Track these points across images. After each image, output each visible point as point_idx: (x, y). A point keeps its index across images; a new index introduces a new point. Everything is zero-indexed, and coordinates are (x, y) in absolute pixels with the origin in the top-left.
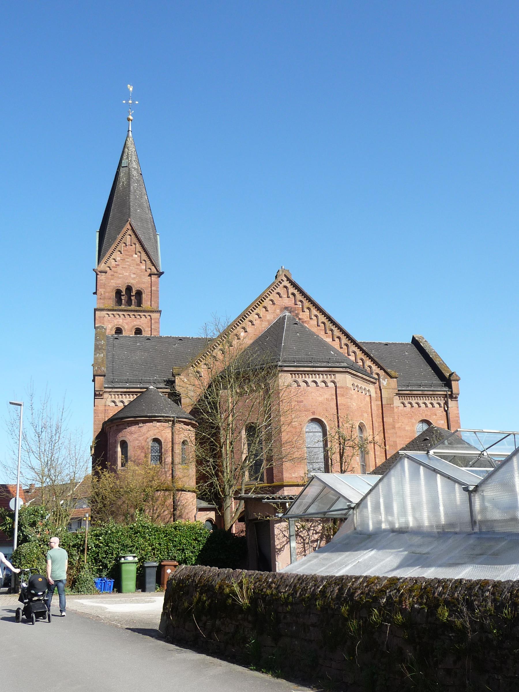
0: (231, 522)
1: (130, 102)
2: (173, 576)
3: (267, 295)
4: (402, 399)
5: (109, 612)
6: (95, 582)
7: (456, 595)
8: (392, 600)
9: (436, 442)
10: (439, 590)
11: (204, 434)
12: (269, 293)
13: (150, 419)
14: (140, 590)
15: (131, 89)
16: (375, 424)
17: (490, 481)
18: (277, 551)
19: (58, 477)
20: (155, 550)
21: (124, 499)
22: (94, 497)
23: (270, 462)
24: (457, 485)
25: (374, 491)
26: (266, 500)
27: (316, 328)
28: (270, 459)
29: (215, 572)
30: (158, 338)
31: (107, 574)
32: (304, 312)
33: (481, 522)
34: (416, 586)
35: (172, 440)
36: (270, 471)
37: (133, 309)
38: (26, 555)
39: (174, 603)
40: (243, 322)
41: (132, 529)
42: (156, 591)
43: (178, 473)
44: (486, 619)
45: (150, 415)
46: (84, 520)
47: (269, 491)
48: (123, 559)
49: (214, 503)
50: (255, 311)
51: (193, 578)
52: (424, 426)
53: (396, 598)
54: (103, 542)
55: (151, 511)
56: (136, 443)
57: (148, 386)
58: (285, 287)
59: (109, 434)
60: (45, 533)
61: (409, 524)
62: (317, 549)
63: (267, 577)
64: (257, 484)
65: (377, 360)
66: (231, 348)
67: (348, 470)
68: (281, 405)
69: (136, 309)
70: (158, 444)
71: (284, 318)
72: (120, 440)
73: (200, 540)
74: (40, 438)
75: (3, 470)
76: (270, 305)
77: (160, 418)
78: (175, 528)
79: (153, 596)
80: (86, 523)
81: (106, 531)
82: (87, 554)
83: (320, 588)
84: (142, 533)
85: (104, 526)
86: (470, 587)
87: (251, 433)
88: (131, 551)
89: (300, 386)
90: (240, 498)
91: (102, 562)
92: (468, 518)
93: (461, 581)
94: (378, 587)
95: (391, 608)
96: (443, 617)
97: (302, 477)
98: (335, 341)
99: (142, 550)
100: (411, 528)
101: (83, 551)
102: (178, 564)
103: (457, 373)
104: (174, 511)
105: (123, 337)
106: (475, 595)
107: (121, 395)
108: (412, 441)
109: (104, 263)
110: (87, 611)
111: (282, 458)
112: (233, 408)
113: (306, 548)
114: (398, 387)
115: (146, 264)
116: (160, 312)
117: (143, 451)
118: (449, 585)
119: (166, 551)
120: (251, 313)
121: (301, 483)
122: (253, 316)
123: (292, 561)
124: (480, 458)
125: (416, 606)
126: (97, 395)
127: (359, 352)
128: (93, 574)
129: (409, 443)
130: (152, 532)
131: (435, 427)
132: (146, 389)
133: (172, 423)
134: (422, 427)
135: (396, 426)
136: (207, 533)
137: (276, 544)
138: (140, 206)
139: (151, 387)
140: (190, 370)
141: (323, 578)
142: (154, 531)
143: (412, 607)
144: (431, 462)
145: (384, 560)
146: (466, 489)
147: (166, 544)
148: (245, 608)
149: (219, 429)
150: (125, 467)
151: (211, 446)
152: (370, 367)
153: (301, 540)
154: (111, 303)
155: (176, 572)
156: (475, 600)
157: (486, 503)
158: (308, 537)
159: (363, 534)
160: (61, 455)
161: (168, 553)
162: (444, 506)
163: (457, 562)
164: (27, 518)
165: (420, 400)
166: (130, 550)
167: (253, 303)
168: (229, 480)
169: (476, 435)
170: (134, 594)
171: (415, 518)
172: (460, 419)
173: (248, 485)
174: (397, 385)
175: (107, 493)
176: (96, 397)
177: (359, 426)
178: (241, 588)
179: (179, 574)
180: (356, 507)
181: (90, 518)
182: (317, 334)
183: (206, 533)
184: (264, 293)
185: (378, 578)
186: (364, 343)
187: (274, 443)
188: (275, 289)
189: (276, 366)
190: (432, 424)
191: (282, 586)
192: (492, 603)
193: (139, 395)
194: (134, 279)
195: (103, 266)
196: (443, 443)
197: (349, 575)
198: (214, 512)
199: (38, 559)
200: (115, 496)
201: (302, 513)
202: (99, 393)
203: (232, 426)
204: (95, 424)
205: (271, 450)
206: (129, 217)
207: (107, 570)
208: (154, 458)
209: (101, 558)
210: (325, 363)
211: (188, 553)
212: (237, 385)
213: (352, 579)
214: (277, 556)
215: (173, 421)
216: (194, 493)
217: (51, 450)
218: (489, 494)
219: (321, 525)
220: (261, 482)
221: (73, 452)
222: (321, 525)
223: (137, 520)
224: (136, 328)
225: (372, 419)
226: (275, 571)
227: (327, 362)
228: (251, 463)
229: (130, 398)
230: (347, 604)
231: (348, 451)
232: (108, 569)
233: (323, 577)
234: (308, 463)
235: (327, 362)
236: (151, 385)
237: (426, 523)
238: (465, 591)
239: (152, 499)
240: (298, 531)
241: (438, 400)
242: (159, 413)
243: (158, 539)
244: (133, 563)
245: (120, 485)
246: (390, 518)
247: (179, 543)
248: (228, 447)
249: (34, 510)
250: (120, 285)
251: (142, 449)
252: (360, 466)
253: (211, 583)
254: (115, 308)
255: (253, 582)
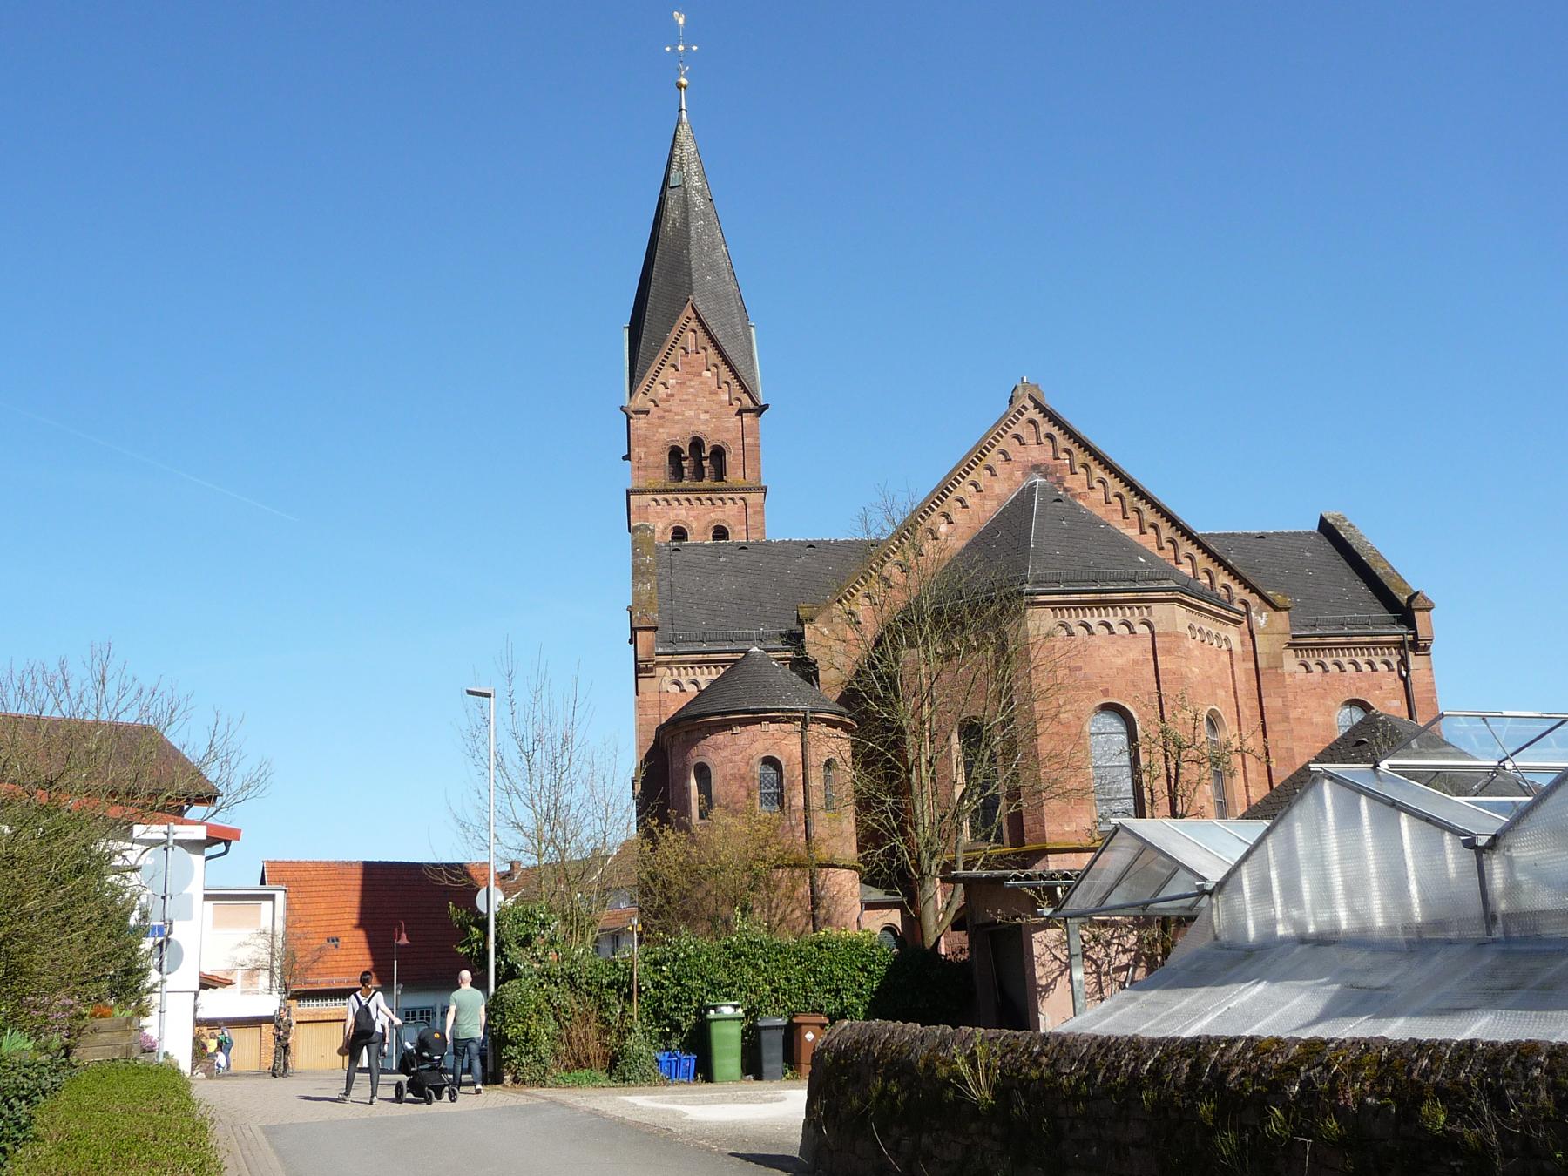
0: (936, 931)
1: (681, 48)
2: (824, 1044)
3: (992, 441)
4: (1303, 656)
5: (692, 1122)
6: (657, 1060)
7: (1462, 1076)
8: (1314, 1087)
9: (1384, 747)
10: (1422, 1065)
11: (871, 744)
12: (996, 436)
13: (755, 716)
14: (751, 1077)
15: (681, 21)
16: (1243, 712)
17: (1525, 824)
18: (1041, 992)
19: (571, 844)
20: (778, 993)
21: (707, 885)
22: (647, 883)
23: (1015, 801)
24: (1447, 837)
25: (1253, 859)
26: (1012, 882)
27: (1103, 508)
28: (1014, 795)
29: (914, 1033)
30: (762, 544)
31: (681, 1044)
32: (1076, 473)
33: (1506, 916)
34: (1366, 1058)
35: (803, 760)
36: (1016, 820)
37: (708, 486)
38: (514, 1004)
39: (829, 1101)
40: (942, 501)
41: (729, 948)
42: (784, 1078)
43: (819, 830)
44: (1537, 1129)
45: (755, 707)
46: (628, 931)
47: (1016, 863)
48: (712, 1012)
49: (898, 891)
50: (969, 478)
51: (867, 1047)
52: (1354, 714)
53: (1324, 1084)
54: (670, 976)
55: (766, 910)
56: (729, 769)
57: (747, 647)
58: (1032, 422)
59: (671, 752)
60: (550, 958)
61: (1340, 924)
62: (1127, 985)
63: (1029, 1043)
64: (990, 848)
65: (1241, 571)
66: (920, 558)
67: (1190, 814)
68: (1033, 677)
69: (713, 487)
70: (775, 769)
71: (1032, 488)
72: (694, 764)
73: (872, 969)
74: (531, 762)
75: (460, 831)
76: (1000, 462)
77: (777, 714)
78: (819, 946)
79: (779, 1089)
80: (633, 937)
81: (675, 954)
82: (638, 1001)
83: (1149, 1063)
84: (750, 957)
85: (670, 944)
86: (1494, 1058)
87: (972, 740)
88: (728, 995)
89: (1073, 634)
90: (955, 880)
91: (669, 1019)
92: (1475, 908)
93: (1471, 1044)
94: (1280, 1061)
95: (1311, 1105)
96: (1435, 1124)
97: (1089, 830)
98: (1145, 533)
99: (751, 992)
100: (1346, 933)
101: (629, 997)
102: (827, 1021)
103: (1426, 594)
104: (812, 909)
105: (689, 545)
106: (1508, 1075)
107: (692, 668)
108: (1328, 747)
109: (644, 393)
110: (645, 1119)
111: (1040, 792)
112: (931, 687)
113: (1103, 985)
114: (1292, 630)
115: (729, 389)
116: (764, 490)
117: (744, 784)
118: (1445, 1054)
119: (802, 994)
120: (959, 483)
121: (1086, 842)
122: (964, 490)
123: (1077, 1010)
124: (1497, 775)
125: (1369, 1100)
126: (642, 670)
127: (1201, 555)
128: (652, 1043)
129: (1322, 752)
130: (770, 955)
131: (1381, 715)
132: (743, 655)
133: (800, 723)
134: (1347, 719)
135: (1291, 716)
136: (887, 955)
137: (1037, 976)
138: (713, 267)
139: (755, 649)
140: (834, 610)
141: (1154, 1043)
142: (774, 953)
143: (1361, 1103)
144: (1385, 785)
145: (1287, 1003)
146: (1470, 844)
147: (800, 980)
148: (983, 1109)
149: (904, 733)
150: (709, 819)
151: (886, 769)
152: (1226, 587)
153: (1091, 966)
154: (661, 477)
155: (829, 1034)
156: (1508, 1086)
157: (1518, 875)
158: (1107, 959)
159: (1234, 949)
160: (576, 797)
161: (806, 997)
162: (1419, 883)
163: (1457, 1004)
164: (513, 928)
165: (1344, 655)
166: (727, 993)
167: (963, 460)
168: (928, 841)
169: (1488, 725)
170: (740, 1085)
171: (1353, 911)
172: (1438, 696)
173: (970, 851)
174: (1288, 625)
175: (672, 875)
176: (639, 675)
177: (1207, 717)
178: (974, 1065)
179: (837, 1039)
180: (1216, 890)
181: (640, 928)
182: (1106, 520)
183: (885, 954)
184: (986, 436)
185: (1278, 1041)
186: (1210, 535)
187: (1022, 759)
188: (1010, 428)
189: (1020, 593)
190: (1373, 709)
191: (1062, 1060)
192: (1548, 1093)
193: (728, 667)
194: (706, 422)
195: (640, 400)
196: (1407, 745)
197: (1212, 1034)
198: (899, 911)
199: (539, 1013)
200: (690, 881)
201: (1093, 906)
202: (647, 665)
203: (931, 726)
204: (639, 731)
205: (1016, 774)
206: (691, 293)
207: (681, 1036)
208: (767, 799)
209: (666, 1010)
210: (1126, 584)
211: (847, 999)
212: (936, 637)
213: (1219, 1044)
214: (1040, 1001)
215: (804, 721)
216: (855, 872)
217: (555, 786)
218: (1524, 854)
219: (1135, 932)
220: (996, 845)
221: (599, 790)
222: (1135, 932)
223: (737, 929)
224: (715, 527)
225: (1237, 703)
226: (1038, 1028)
227: (1131, 580)
228: (975, 803)
229: (710, 673)
230: (1210, 1098)
231: (1189, 772)
232: (682, 1033)
233: (1154, 1039)
234: (1098, 800)
235: (1131, 580)
236: (754, 644)
237: (1380, 922)
238: (1484, 1066)
239: (767, 886)
240: (1084, 946)
241: (1384, 654)
242: (774, 704)
243: (784, 970)
244: (734, 1019)
245: (698, 857)
246: (1295, 913)
247: (829, 976)
248: (923, 770)
249: (527, 911)
250: (678, 438)
251: (741, 782)
252: (1213, 805)
253: (908, 1056)
254: (669, 487)
255: (999, 1053)
